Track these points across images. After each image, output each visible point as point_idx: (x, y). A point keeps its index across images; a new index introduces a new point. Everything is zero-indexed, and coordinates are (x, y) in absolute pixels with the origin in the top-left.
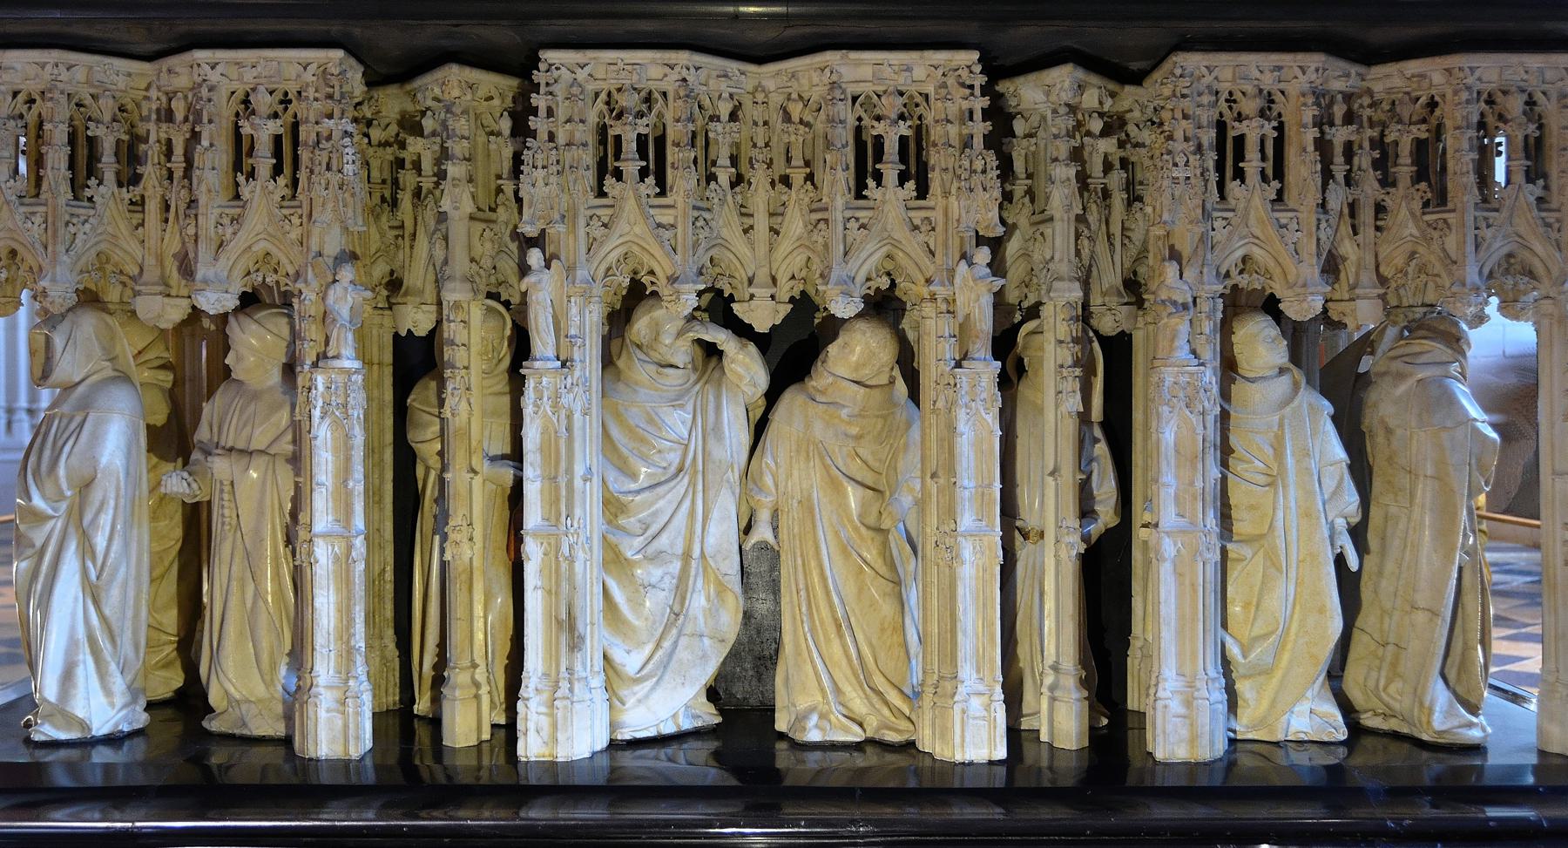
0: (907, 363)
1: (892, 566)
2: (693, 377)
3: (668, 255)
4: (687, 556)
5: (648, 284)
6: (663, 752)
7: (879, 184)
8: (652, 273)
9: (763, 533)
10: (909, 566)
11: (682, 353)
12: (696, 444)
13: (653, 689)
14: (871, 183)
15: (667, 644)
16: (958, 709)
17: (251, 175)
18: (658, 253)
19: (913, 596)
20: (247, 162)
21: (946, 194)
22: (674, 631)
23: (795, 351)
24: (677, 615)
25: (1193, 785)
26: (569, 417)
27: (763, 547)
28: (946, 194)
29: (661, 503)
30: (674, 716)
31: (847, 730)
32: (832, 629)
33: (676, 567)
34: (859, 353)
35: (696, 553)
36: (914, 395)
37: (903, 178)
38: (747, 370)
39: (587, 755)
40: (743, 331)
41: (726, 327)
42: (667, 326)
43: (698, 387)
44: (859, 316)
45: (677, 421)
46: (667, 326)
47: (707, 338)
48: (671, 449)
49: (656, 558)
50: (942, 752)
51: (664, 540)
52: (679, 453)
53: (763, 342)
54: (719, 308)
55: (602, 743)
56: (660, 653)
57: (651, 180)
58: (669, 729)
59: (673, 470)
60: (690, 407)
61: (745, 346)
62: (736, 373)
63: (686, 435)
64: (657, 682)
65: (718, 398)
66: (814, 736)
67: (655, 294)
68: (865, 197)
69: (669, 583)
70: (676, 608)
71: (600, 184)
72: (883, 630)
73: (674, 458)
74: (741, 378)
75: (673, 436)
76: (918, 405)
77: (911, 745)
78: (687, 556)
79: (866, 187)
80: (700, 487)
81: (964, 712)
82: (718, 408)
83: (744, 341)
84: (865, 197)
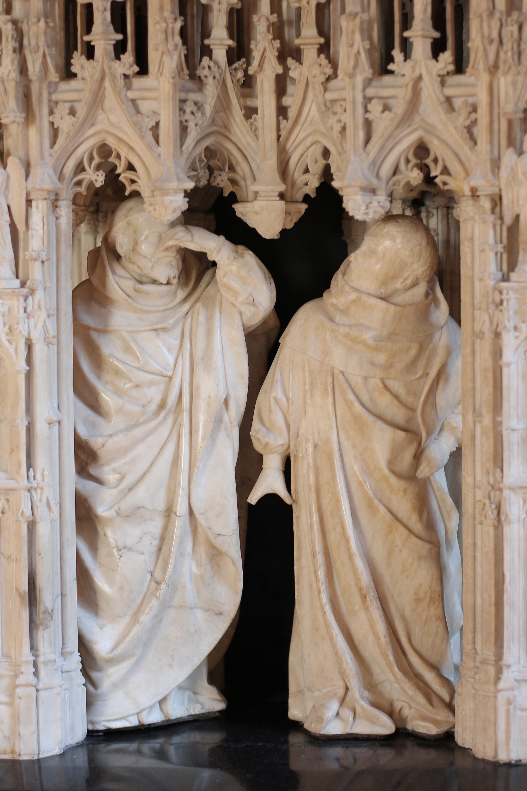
0: (446, 274)
1: (430, 526)
2: (181, 294)
3: (150, 148)
4: (169, 512)
5: (127, 183)
6: (147, 746)
7: (407, 56)
8: (131, 167)
9: (270, 482)
10: (448, 522)
11: (166, 269)
12: (181, 376)
13: (131, 671)
14: (397, 54)
15: (145, 618)
16: (502, 698)
17: (90, 52)
18: (139, 146)
19: (452, 561)
20: (81, 38)
21: (494, 69)
22: (154, 603)
23: (308, 255)
24: (158, 583)
25: (225, 692)
26: (29, 347)
27: (270, 499)
28: (494, 69)
29: (140, 449)
30: (162, 702)
31: (372, 721)
32: (358, 599)
33: (156, 525)
34: (382, 259)
35: (181, 508)
36: (455, 313)
37: (437, 48)
38: (245, 286)
39: (57, 751)
40: (241, 235)
41: (218, 232)
42: (152, 228)
43: (186, 307)
44: (389, 218)
45: (160, 352)
46: (152, 228)
47: (193, 246)
48: (151, 383)
49: (133, 515)
50: (483, 750)
51: (141, 495)
52: (162, 387)
53: (269, 253)
54: (214, 208)
55: (80, 735)
56: (137, 629)
57: (129, 57)
58: (154, 717)
59: (153, 407)
60: (177, 332)
61: (242, 256)
62: (229, 288)
63: (171, 360)
64: (137, 663)
65: (210, 319)
66: (334, 728)
67: (136, 194)
68: (392, 72)
69: (149, 545)
70: (158, 575)
71: (68, 64)
72: (418, 600)
73: (154, 394)
74: (235, 293)
75: (156, 367)
76: (460, 325)
77: (446, 740)
78: (169, 512)
79: (391, 59)
80: (185, 430)
81: (509, 703)
82: (209, 332)
83: (241, 248)
84: (392, 72)
